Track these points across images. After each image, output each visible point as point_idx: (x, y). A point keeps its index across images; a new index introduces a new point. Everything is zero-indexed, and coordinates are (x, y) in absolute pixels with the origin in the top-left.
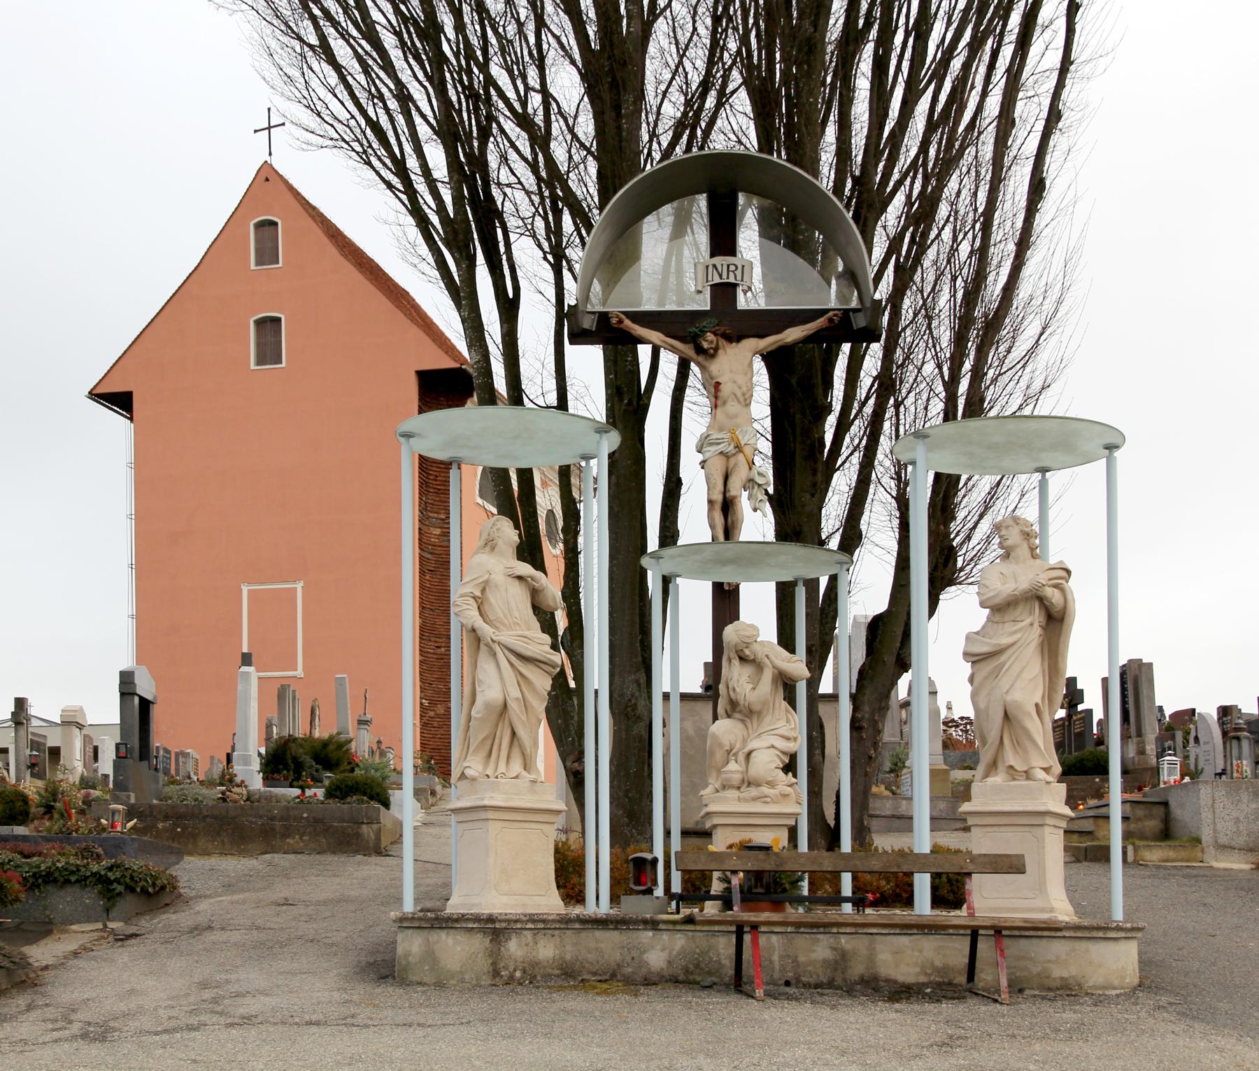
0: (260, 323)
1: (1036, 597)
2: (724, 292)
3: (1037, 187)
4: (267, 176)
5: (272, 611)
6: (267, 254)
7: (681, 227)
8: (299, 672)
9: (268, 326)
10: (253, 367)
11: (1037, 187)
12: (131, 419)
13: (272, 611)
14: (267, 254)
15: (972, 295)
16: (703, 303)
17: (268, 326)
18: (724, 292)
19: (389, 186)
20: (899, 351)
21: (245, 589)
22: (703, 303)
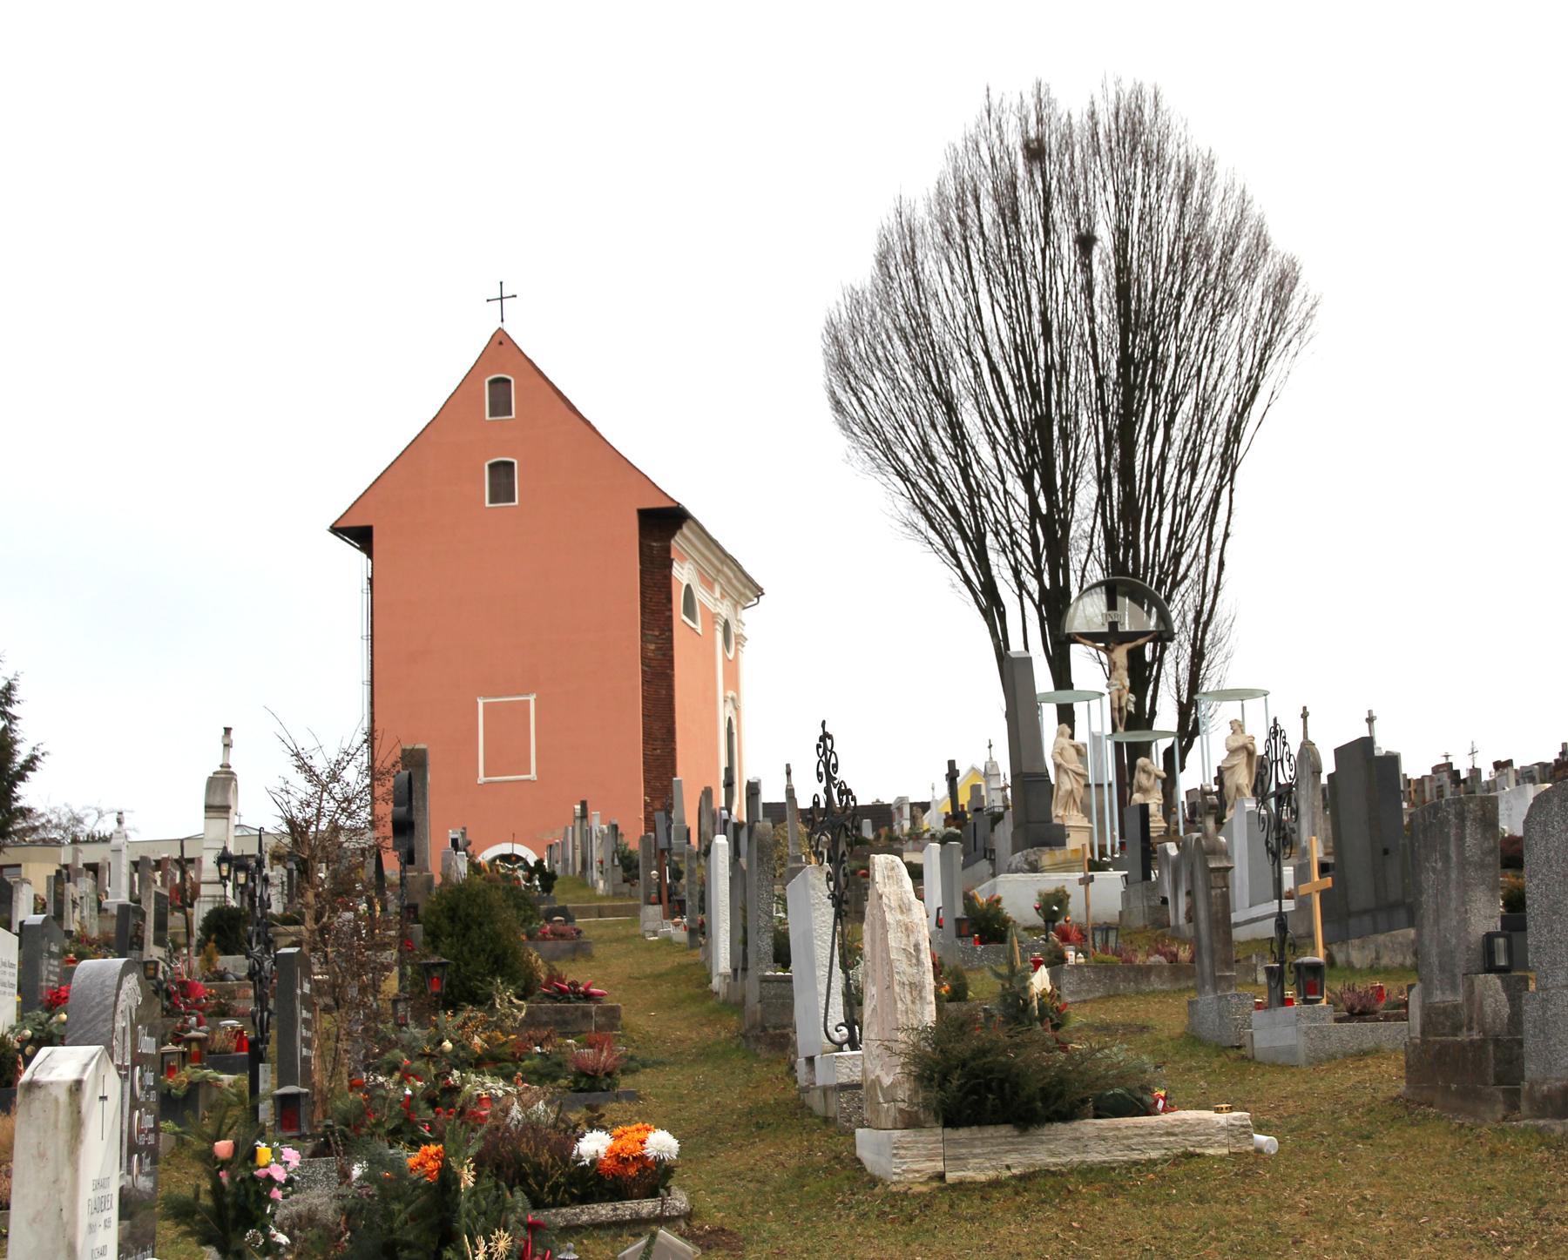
0: (494, 467)
1: (1244, 747)
2: (1113, 625)
3: (1221, 565)
4: (501, 341)
5: (507, 723)
6: (500, 404)
7: (1496, 1013)
8: (533, 775)
9: (502, 472)
10: (487, 504)
11: (1221, 565)
12: (370, 556)
13: (507, 723)
14: (500, 404)
15: (1199, 614)
16: (1106, 629)
17: (502, 472)
18: (1113, 625)
19: (967, 581)
20: (1317, 851)
21: (481, 702)
22: (1106, 629)
